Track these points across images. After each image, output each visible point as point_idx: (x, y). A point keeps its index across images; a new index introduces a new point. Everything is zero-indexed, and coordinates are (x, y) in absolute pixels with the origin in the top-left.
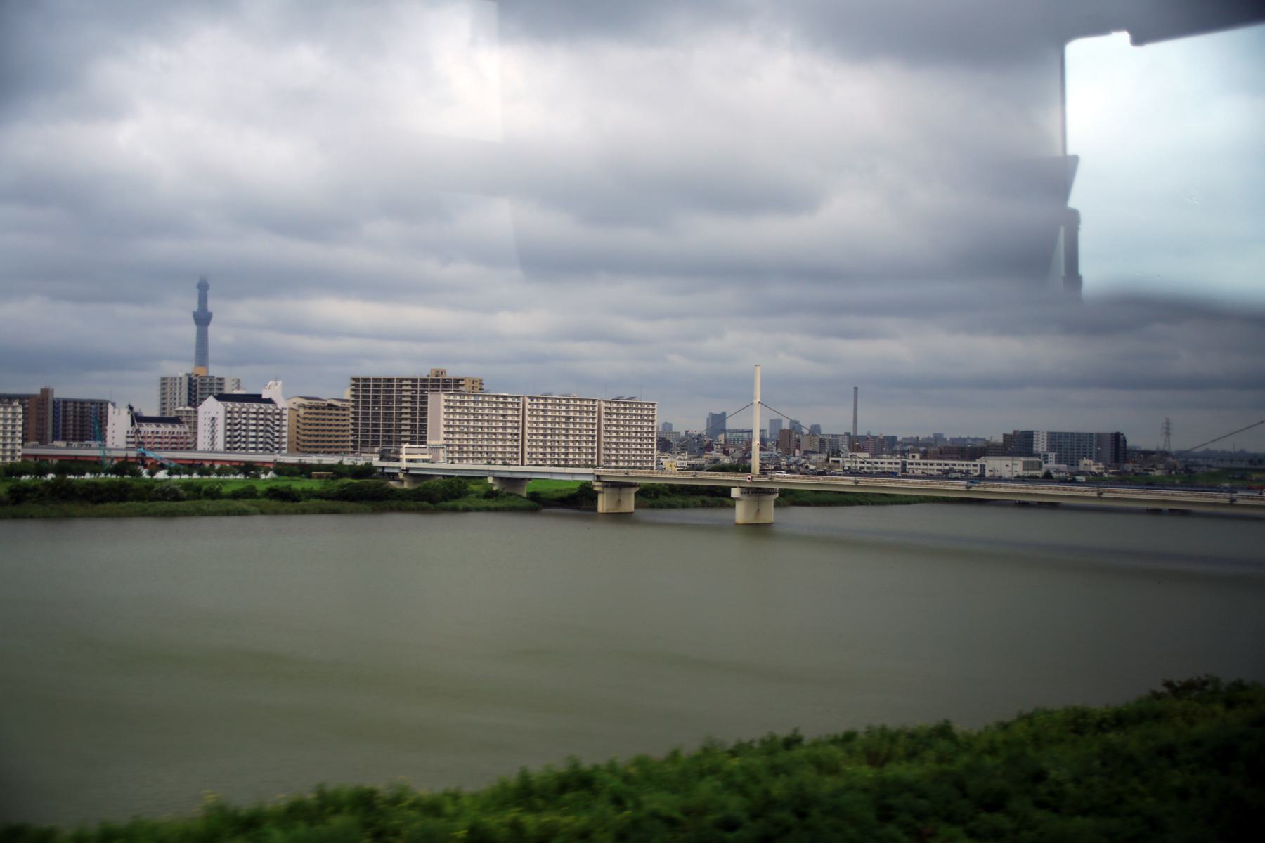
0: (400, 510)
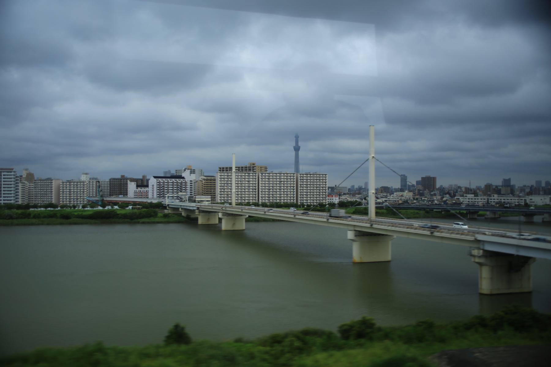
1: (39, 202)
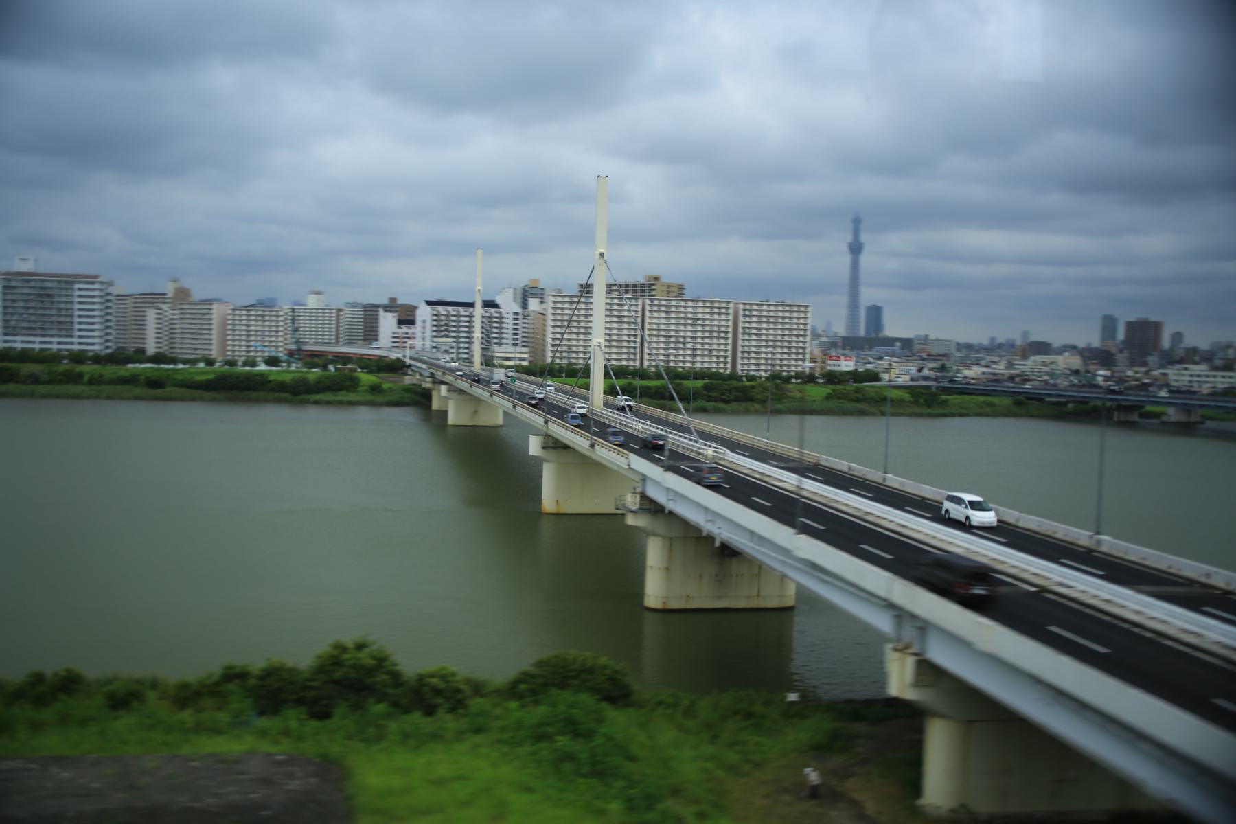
0: (280, 401)
1: (185, 351)
